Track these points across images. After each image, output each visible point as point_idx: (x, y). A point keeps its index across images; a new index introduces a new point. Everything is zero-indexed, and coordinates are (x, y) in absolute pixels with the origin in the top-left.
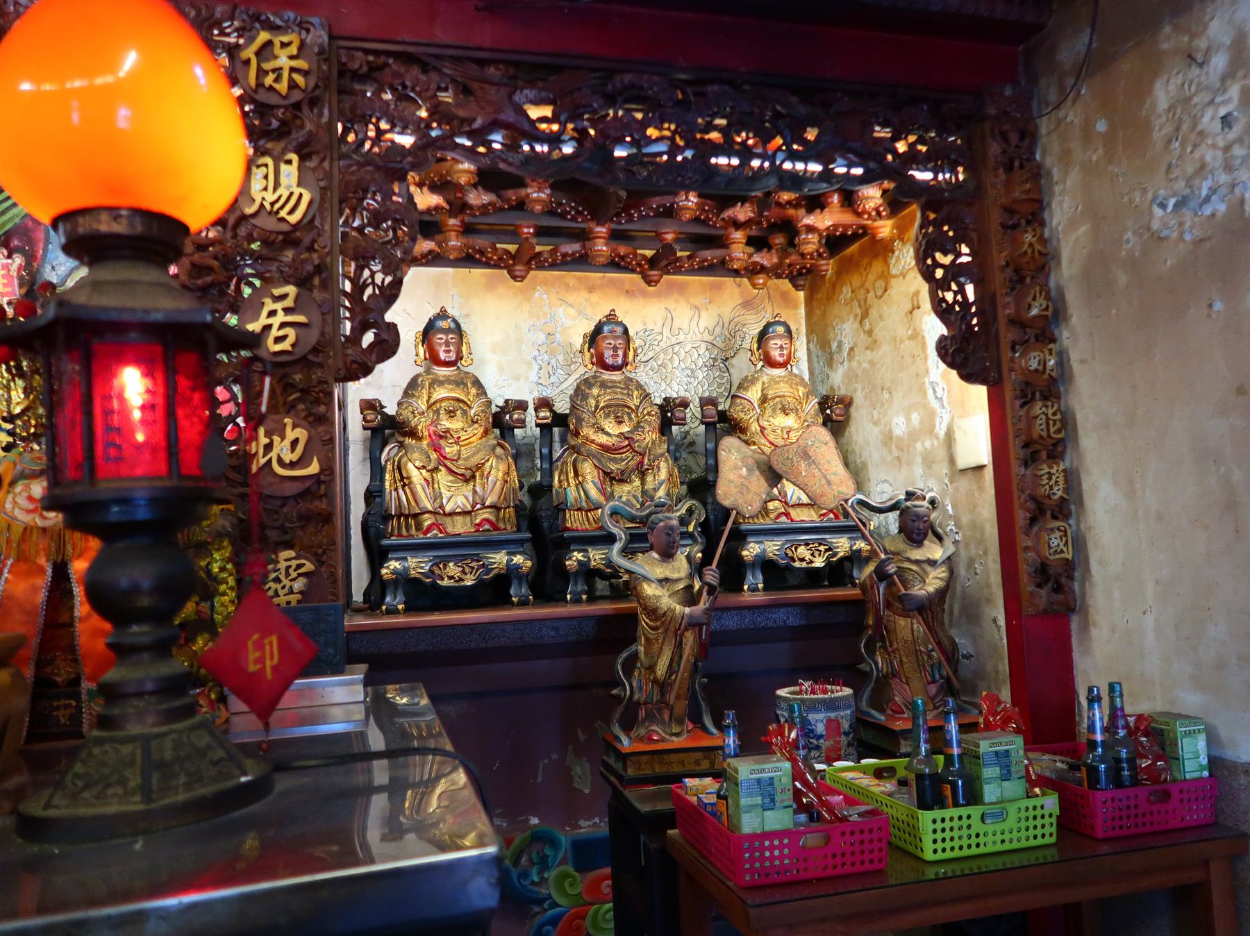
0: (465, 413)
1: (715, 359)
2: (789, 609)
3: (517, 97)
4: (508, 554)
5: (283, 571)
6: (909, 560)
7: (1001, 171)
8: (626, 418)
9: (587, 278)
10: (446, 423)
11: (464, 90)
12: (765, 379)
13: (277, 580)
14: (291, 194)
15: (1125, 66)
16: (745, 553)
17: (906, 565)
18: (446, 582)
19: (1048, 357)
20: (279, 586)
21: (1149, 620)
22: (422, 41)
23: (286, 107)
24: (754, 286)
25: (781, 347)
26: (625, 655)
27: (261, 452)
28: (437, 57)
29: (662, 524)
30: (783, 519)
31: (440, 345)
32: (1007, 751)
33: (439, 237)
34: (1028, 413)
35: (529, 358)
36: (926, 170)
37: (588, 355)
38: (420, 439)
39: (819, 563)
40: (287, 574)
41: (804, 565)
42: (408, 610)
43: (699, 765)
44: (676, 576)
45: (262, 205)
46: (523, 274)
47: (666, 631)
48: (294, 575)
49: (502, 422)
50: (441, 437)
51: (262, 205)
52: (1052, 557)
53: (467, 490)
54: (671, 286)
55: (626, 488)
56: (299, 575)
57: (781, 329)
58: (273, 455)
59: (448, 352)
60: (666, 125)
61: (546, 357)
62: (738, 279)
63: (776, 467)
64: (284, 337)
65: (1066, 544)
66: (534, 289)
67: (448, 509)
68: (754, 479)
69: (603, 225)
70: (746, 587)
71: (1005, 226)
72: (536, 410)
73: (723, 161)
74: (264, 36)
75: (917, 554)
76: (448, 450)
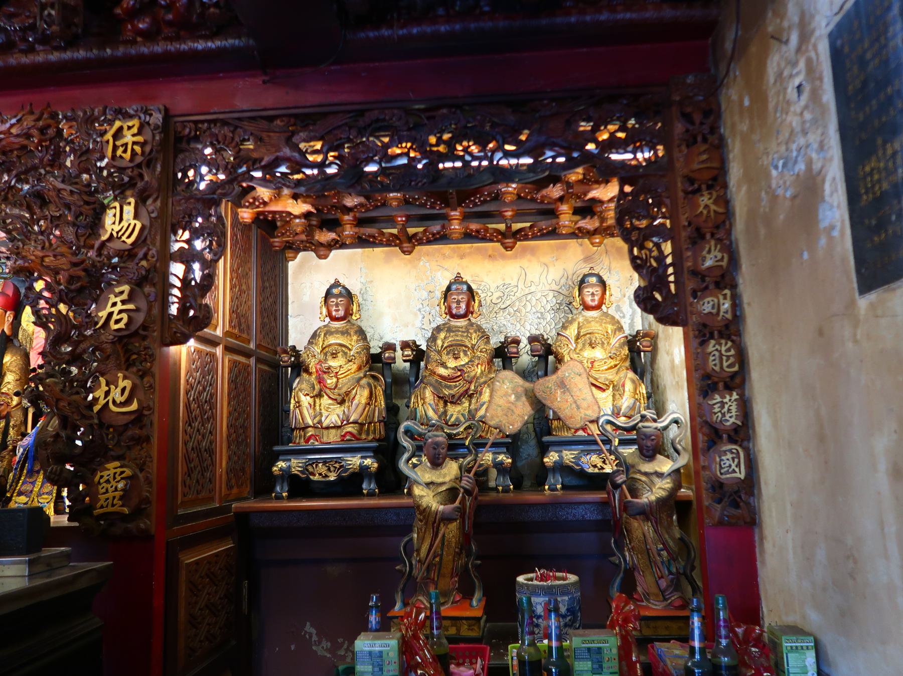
1: (560, 304)
2: (587, 506)
3: (294, 140)
5: (112, 476)
6: (640, 472)
7: (684, 147)
8: (462, 354)
11: (259, 140)
12: (581, 319)
13: (108, 481)
14: (129, 225)
15: (753, 49)
16: (546, 460)
18: (316, 478)
19: (722, 301)
20: (109, 486)
21: (790, 535)
22: (227, 110)
23: (132, 167)
24: (592, 244)
25: (593, 294)
26: (406, 539)
27: (103, 396)
28: (239, 119)
30: (581, 433)
32: (600, 648)
33: (339, 229)
36: (626, 152)
37: (443, 307)
38: (310, 374)
40: (114, 478)
41: (596, 471)
42: (291, 497)
44: (440, 480)
45: (111, 234)
46: (409, 249)
48: (118, 478)
49: (376, 362)
50: (325, 373)
51: (111, 234)
52: (724, 477)
55: (459, 408)
56: (122, 479)
57: (593, 280)
58: (110, 398)
59: (337, 311)
60: (404, 145)
61: (428, 309)
62: (580, 240)
63: (537, 394)
64: (121, 319)
65: (738, 465)
67: (324, 425)
68: (519, 404)
69: (456, 210)
70: (547, 487)
71: (686, 193)
72: (402, 349)
73: (449, 165)
74: (118, 124)
75: (647, 467)
76: (329, 381)
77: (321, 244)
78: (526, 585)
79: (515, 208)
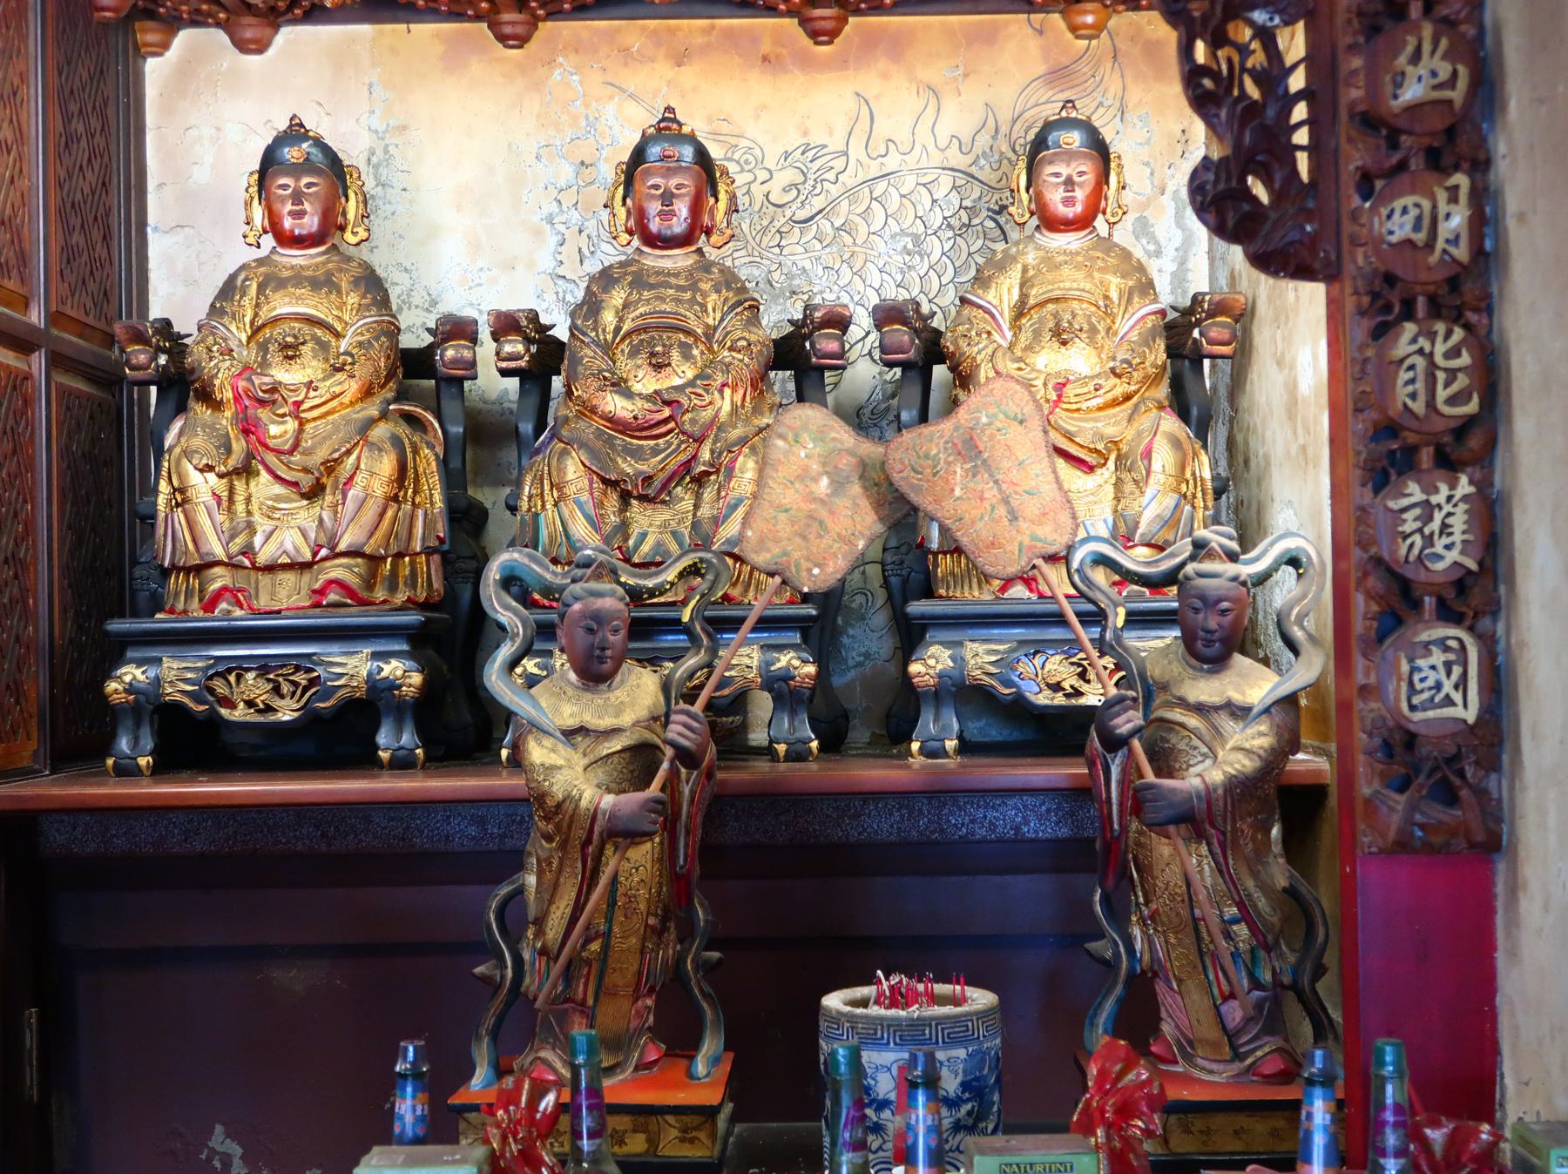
0: (323, 346)
1: (972, 211)
4: (766, 648)
6: (1182, 703)
9: (672, 32)
10: (285, 374)
12: (1031, 257)
17: (1177, 715)
18: (239, 714)
19: (1443, 207)
24: (1073, 29)
25: (1069, 183)
29: (577, 607)
31: (283, 199)
34: (1380, 355)
35: (536, 219)
38: (217, 406)
39: (286, 713)
41: (1060, 700)
43: (621, 1143)
46: (520, 30)
47: (564, 846)
49: (417, 374)
50: (262, 403)
53: (306, 516)
54: (870, 43)
55: (662, 515)
57: (1074, 138)
61: (575, 216)
62: (1037, 18)
63: (896, 477)
66: (550, 63)
67: (262, 559)
68: (842, 503)
72: (496, 337)
75: (1204, 690)
76: (274, 430)
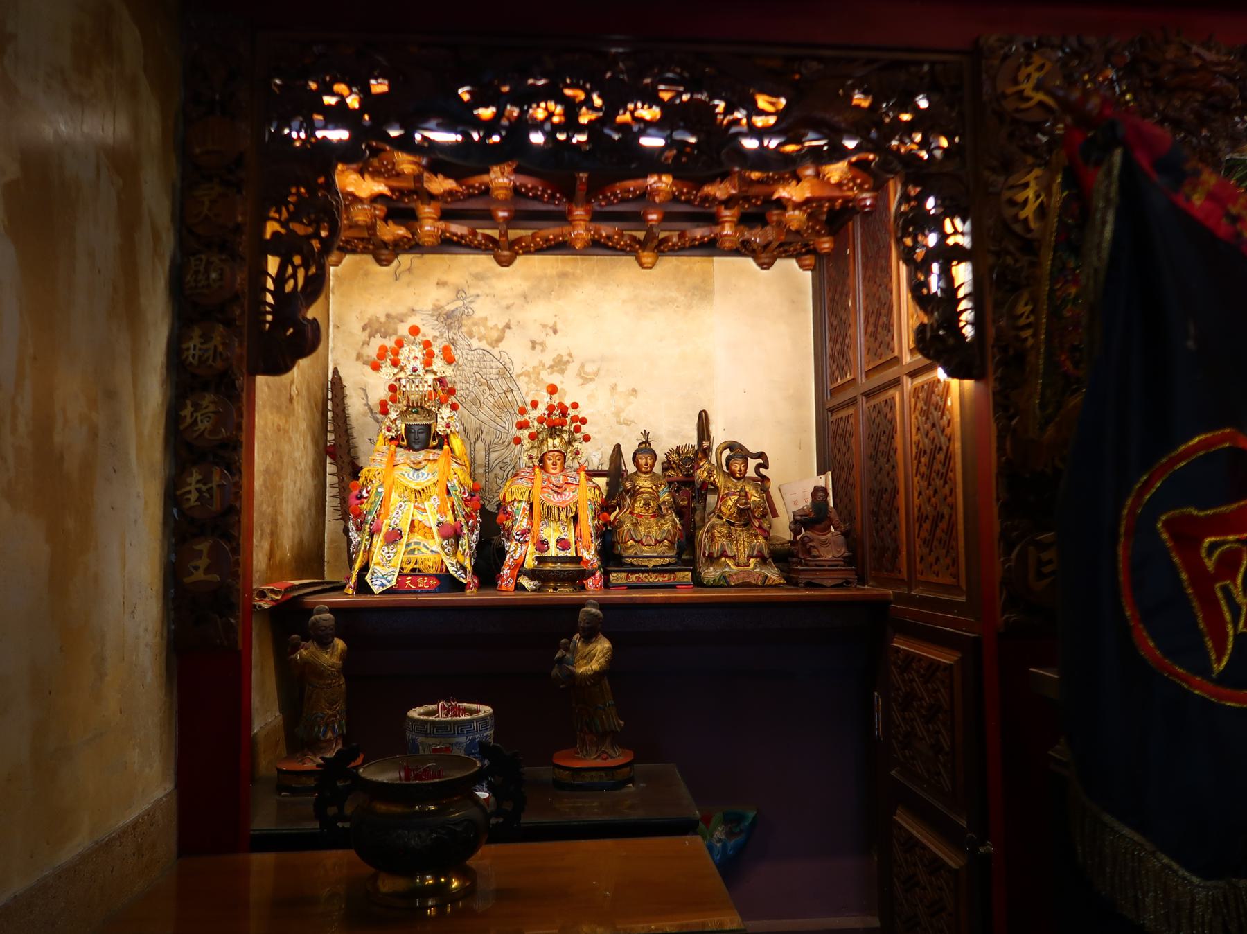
24: (801, 266)
77: (385, 245)
78: (426, 722)
79: (512, 208)
